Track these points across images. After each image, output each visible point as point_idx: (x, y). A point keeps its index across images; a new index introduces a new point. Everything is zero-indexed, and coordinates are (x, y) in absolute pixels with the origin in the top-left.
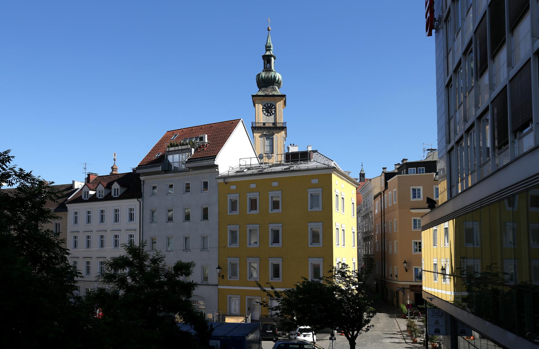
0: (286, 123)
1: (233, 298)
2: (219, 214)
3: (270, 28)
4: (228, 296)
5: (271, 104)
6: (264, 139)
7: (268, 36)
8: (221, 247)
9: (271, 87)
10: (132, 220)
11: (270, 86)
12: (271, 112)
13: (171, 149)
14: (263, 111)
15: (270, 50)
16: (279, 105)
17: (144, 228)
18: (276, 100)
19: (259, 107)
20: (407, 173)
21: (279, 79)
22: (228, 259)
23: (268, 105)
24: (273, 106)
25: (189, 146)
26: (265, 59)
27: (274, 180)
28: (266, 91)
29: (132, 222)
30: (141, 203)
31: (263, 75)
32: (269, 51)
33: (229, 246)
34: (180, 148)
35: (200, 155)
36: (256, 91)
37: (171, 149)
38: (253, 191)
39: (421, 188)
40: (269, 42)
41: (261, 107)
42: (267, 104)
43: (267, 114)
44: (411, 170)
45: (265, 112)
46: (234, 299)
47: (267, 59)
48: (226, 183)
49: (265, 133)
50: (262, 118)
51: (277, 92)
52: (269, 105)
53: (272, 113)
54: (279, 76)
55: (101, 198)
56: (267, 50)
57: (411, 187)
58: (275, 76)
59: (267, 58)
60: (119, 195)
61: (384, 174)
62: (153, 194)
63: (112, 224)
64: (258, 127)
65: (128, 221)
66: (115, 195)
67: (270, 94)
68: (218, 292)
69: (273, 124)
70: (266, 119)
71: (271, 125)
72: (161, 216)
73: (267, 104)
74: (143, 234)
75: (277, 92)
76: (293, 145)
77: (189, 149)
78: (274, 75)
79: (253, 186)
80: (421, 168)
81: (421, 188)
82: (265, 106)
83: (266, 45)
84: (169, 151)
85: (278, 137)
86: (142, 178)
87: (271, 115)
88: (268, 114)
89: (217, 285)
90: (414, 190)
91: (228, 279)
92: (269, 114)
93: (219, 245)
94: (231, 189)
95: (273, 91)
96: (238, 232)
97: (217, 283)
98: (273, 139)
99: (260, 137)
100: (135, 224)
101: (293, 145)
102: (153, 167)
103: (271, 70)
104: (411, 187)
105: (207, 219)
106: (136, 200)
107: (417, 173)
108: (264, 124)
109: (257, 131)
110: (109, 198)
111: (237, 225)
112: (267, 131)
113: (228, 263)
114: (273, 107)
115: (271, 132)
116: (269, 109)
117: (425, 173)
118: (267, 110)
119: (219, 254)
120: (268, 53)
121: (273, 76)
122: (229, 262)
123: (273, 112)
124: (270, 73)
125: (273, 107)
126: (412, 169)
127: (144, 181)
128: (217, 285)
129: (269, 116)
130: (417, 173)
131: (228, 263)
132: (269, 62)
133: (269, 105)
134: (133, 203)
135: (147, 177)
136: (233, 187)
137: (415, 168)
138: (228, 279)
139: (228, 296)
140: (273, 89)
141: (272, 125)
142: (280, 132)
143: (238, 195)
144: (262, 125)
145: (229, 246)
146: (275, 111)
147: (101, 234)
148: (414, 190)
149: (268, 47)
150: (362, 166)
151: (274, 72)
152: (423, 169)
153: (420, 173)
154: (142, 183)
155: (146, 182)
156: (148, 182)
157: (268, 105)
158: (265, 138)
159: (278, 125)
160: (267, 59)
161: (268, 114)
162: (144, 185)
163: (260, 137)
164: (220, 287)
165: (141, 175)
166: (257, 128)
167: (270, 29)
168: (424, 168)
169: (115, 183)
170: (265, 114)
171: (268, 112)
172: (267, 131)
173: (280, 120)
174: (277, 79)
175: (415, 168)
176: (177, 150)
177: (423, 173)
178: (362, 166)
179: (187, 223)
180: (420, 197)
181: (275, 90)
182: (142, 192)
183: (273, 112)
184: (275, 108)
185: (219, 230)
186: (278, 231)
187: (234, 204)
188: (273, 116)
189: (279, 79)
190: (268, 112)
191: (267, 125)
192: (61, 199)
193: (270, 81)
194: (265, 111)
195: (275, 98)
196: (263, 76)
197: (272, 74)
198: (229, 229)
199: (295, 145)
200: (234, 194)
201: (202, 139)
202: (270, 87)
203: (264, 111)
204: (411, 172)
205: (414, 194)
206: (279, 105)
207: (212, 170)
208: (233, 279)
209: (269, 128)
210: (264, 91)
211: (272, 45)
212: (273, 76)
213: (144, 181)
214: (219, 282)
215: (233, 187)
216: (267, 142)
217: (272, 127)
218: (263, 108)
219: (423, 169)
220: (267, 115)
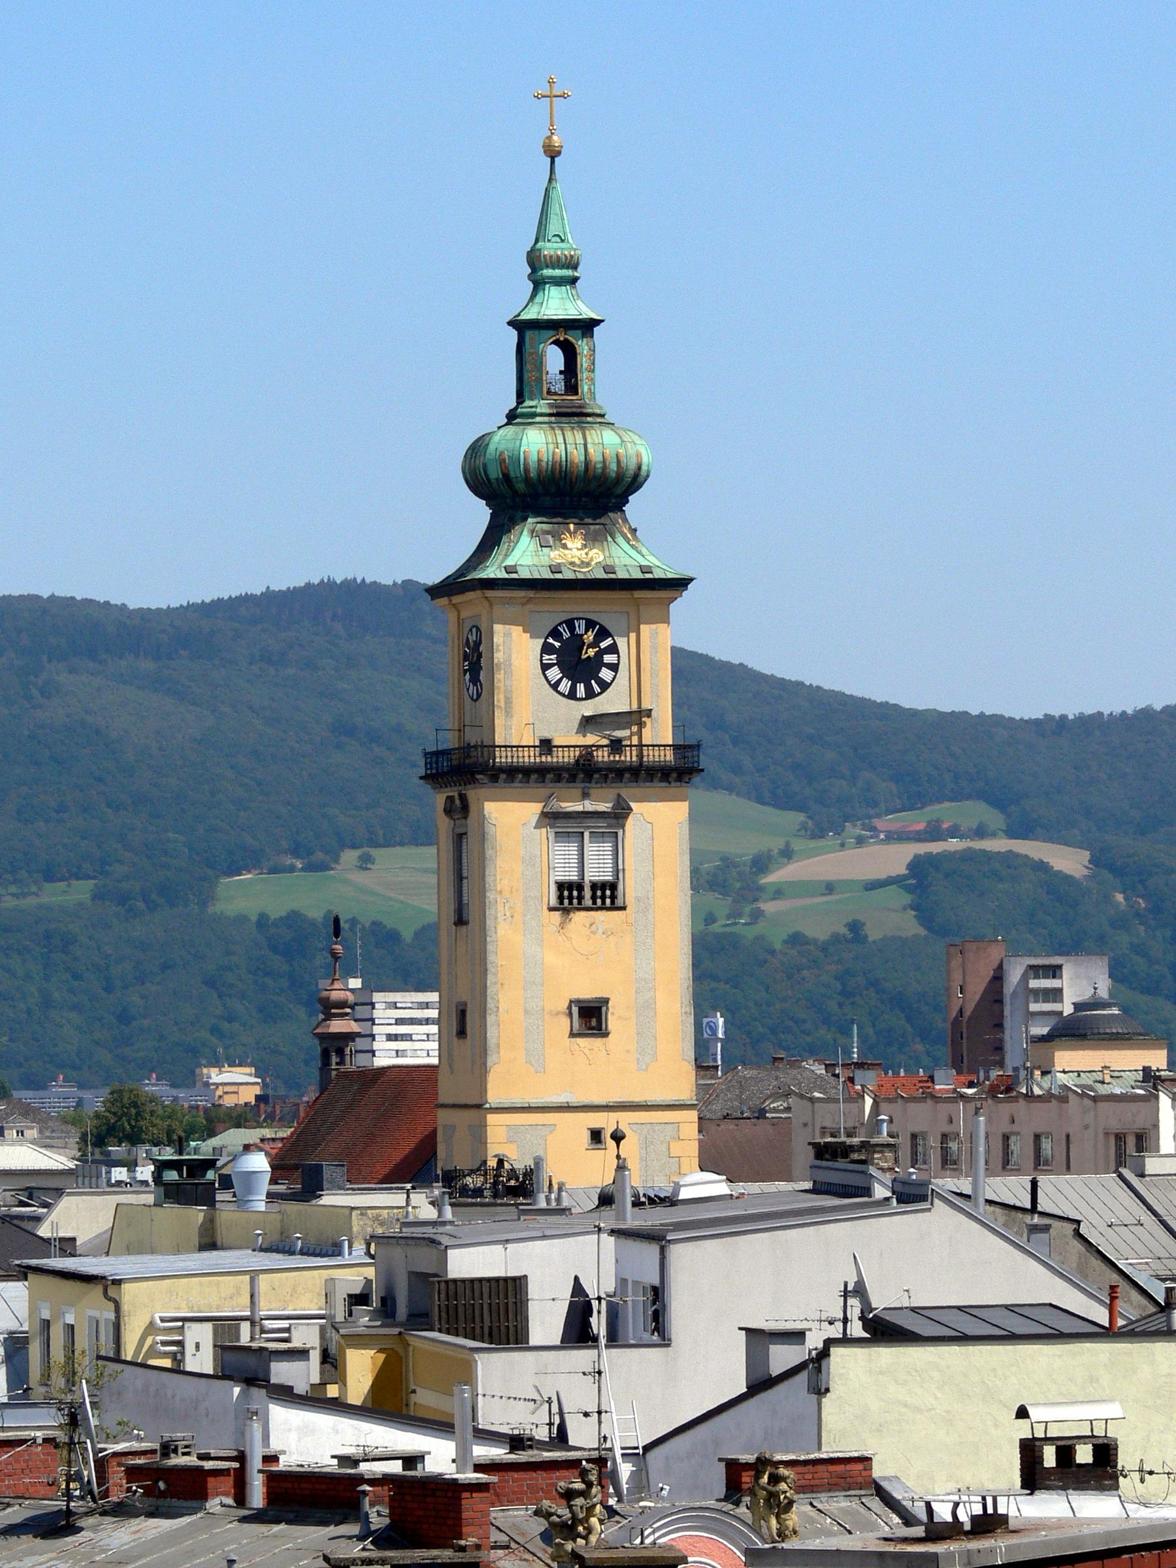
42: (614, 668)
43: (565, 686)
45: (554, 673)
82: (555, 633)
144: (529, 758)
170: (555, 686)
203: (550, 666)
218: (546, 649)
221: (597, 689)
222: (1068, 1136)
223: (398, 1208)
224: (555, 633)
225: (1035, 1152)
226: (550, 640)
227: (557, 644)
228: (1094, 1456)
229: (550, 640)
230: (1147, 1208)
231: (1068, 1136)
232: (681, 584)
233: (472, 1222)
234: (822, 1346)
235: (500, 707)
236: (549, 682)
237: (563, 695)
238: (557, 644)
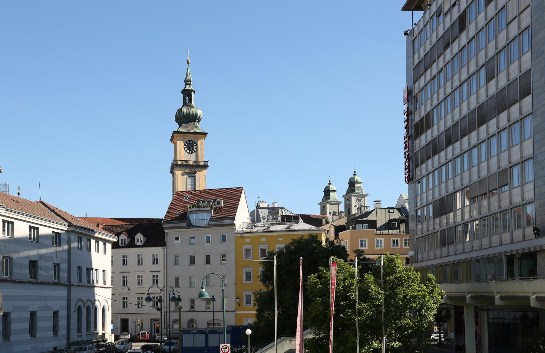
0: (208, 162)
1: (247, 320)
2: (236, 259)
3: (189, 61)
4: (244, 318)
5: (192, 141)
6: (186, 177)
7: (188, 69)
8: (238, 283)
9: (192, 123)
10: (155, 263)
11: (191, 122)
12: (193, 149)
13: (193, 209)
14: (184, 148)
15: (189, 84)
16: (201, 143)
17: (168, 270)
18: (198, 138)
19: (181, 144)
20: (355, 228)
21: (200, 116)
22: (244, 292)
23: (189, 142)
24: (195, 143)
25: (209, 208)
26: (185, 93)
27: (280, 236)
28: (187, 127)
29: (155, 265)
30: (165, 250)
31: (185, 110)
32: (189, 86)
33: (244, 283)
34: (201, 209)
35: (219, 215)
36: (175, 127)
37: (193, 209)
38: (263, 243)
39: (366, 240)
40: (188, 75)
41: (183, 144)
42: (189, 141)
43: (188, 151)
44: (358, 226)
45: (186, 149)
46: (248, 320)
47: (187, 94)
48: (242, 237)
49: (187, 171)
50: (184, 156)
51: (198, 129)
52: (191, 142)
53: (194, 151)
54: (200, 113)
55: (123, 245)
56: (186, 85)
57: (359, 239)
58: (197, 112)
59: (187, 92)
60: (126, 244)
61: (334, 226)
62: (190, 243)
63: (151, 266)
64: (180, 164)
65: (152, 264)
66: (122, 244)
67: (192, 131)
68: (236, 316)
69: (195, 162)
70: (188, 157)
71: (193, 163)
72: (185, 260)
73: (189, 141)
74: (167, 274)
75: (198, 129)
76: (263, 201)
77: (210, 210)
78: (196, 112)
79: (264, 240)
80: (366, 225)
81: (366, 240)
82: (186, 143)
83: (185, 79)
84: (191, 211)
85: (200, 175)
86: (166, 231)
87: (192, 153)
88: (189, 152)
89: (235, 311)
90: (361, 241)
91: (244, 306)
92: (191, 152)
93: (236, 282)
94: (246, 241)
95: (194, 127)
96: (252, 273)
97: (234, 310)
98: (195, 177)
99: (182, 175)
100: (160, 266)
101: (263, 201)
102: (179, 223)
103: (191, 106)
104: (359, 239)
105: (210, 263)
106: (161, 248)
107: (363, 229)
108: (186, 161)
109: (179, 169)
110: (132, 244)
111: (251, 267)
112: (189, 169)
113: (244, 295)
114: (195, 145)
115: (193, 170)
116: (191, 146)
117: (369, 229)
118: (188, 147)
119: (236, 288)
120: (188, 88)
121: (194, 113)
122: (244, 294)
123: (195, 150)
124: (191, 109)
125: (195, 145)
126: (359, 225)
127: (167, 233)
128: (235, 311)
129: (191, 154)
130: (363, 229)
131: (244, 295)
132: (190, 96)
133: (191, 142)
134: (158, 251)
135: (171, 230)
136: (248, 240)
137: (362, 225)
138: (244, 306)
139: (244, 318)
140: (194, 126)
141: (193, 163)
142: (203, 171)
143: (252, 246)
144: (183, 163)
145: (244, 283)
146: (197, 149)
147: (138, 275)
148: (361, 241)
149: (187, 81)
150: (259, 198)
151: (195, 108)
152: (367, 226)
153: (365, 229)
154: (166, 235)
155: (169, 234)
156: (170, 234)
157: (189, 142)
158: (187, 176)
159: (200, 163)
160: (187, 94)
161: (189, 152)
162: (168, 236)
163: (182, 175)
164: (237, 312)
165: (165, 228)
166: (179, 166)
167: (189, 62)
168: (368, 225)
169: (138, 234)
170: (186, 151)
171: (190, 150)
172: (189, 169)
173: (202, 158)
174: (199, 115)
175: (362, 225)
176: (199, 211)
177: (367, 229)
178: (259, 198)
179: (208, 266)
180: (366, 247)
181: (196, 127)
182: (166, 241)
183: (195, 150)
184: (196, 146)
185: (236, 271)
186: (250, 272)
187: (248, 251)
188: (194, 154)
189: (200, 116)
190: (190, 149)
191: (189, 163)
192: (538, 268)
193: (191, 117)
194: (187, 148)
195: (197, 135)
196: (185, 112)
197: (193, 110)
198: (244, 271)
199: (264, 201)
200: (249, 245)
201: (218, 203)
202: (191, 123)
203: (185, 148)
204: (358, 228)
205: (361, 244)
206: (201, 143)
207: (231, 227)
208: (248, 306)
209: (190, 166)
210: (185, 127)
211: (192, 79)
212: (194, 113)
213: (167, 233)
214: (236, 308)
215: (248, 240)
216: (189, 180)
217: (194, 165)
218: (185, 145)
219: (367, 226)
220: (189, 153)
221: (194, 152)
222: (19, 187)
223: (124, 234)
224: (186, 143)
225: (60, 215)
226: (185, 144)
227: (187, 144)
228: (213, 347)
229: (185, 144)
230: (89, 286)
231: (19, 187)
232: (206, 134)
233: (239, 235)
234: (364, 213)
235: (356, 267)
236: (185, 151)
237: (188, 153)
238: (187, 144)
